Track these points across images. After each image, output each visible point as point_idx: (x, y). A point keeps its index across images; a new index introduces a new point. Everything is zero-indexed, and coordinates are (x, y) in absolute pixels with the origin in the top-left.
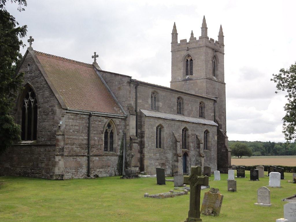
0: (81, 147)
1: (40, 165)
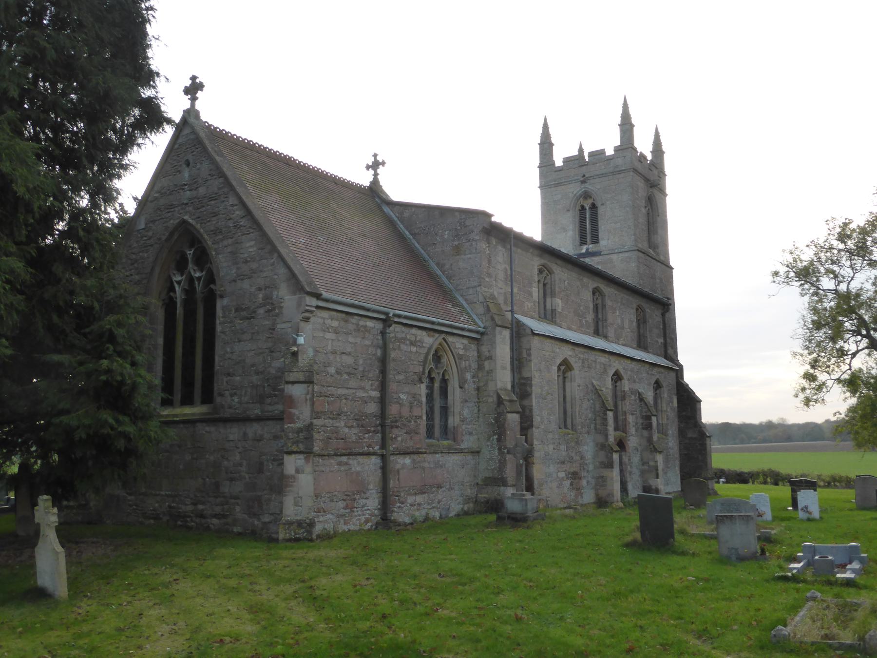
0: (362, 426)
1: (226, 489)
